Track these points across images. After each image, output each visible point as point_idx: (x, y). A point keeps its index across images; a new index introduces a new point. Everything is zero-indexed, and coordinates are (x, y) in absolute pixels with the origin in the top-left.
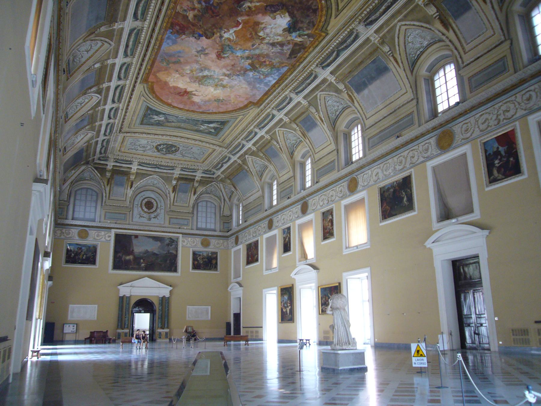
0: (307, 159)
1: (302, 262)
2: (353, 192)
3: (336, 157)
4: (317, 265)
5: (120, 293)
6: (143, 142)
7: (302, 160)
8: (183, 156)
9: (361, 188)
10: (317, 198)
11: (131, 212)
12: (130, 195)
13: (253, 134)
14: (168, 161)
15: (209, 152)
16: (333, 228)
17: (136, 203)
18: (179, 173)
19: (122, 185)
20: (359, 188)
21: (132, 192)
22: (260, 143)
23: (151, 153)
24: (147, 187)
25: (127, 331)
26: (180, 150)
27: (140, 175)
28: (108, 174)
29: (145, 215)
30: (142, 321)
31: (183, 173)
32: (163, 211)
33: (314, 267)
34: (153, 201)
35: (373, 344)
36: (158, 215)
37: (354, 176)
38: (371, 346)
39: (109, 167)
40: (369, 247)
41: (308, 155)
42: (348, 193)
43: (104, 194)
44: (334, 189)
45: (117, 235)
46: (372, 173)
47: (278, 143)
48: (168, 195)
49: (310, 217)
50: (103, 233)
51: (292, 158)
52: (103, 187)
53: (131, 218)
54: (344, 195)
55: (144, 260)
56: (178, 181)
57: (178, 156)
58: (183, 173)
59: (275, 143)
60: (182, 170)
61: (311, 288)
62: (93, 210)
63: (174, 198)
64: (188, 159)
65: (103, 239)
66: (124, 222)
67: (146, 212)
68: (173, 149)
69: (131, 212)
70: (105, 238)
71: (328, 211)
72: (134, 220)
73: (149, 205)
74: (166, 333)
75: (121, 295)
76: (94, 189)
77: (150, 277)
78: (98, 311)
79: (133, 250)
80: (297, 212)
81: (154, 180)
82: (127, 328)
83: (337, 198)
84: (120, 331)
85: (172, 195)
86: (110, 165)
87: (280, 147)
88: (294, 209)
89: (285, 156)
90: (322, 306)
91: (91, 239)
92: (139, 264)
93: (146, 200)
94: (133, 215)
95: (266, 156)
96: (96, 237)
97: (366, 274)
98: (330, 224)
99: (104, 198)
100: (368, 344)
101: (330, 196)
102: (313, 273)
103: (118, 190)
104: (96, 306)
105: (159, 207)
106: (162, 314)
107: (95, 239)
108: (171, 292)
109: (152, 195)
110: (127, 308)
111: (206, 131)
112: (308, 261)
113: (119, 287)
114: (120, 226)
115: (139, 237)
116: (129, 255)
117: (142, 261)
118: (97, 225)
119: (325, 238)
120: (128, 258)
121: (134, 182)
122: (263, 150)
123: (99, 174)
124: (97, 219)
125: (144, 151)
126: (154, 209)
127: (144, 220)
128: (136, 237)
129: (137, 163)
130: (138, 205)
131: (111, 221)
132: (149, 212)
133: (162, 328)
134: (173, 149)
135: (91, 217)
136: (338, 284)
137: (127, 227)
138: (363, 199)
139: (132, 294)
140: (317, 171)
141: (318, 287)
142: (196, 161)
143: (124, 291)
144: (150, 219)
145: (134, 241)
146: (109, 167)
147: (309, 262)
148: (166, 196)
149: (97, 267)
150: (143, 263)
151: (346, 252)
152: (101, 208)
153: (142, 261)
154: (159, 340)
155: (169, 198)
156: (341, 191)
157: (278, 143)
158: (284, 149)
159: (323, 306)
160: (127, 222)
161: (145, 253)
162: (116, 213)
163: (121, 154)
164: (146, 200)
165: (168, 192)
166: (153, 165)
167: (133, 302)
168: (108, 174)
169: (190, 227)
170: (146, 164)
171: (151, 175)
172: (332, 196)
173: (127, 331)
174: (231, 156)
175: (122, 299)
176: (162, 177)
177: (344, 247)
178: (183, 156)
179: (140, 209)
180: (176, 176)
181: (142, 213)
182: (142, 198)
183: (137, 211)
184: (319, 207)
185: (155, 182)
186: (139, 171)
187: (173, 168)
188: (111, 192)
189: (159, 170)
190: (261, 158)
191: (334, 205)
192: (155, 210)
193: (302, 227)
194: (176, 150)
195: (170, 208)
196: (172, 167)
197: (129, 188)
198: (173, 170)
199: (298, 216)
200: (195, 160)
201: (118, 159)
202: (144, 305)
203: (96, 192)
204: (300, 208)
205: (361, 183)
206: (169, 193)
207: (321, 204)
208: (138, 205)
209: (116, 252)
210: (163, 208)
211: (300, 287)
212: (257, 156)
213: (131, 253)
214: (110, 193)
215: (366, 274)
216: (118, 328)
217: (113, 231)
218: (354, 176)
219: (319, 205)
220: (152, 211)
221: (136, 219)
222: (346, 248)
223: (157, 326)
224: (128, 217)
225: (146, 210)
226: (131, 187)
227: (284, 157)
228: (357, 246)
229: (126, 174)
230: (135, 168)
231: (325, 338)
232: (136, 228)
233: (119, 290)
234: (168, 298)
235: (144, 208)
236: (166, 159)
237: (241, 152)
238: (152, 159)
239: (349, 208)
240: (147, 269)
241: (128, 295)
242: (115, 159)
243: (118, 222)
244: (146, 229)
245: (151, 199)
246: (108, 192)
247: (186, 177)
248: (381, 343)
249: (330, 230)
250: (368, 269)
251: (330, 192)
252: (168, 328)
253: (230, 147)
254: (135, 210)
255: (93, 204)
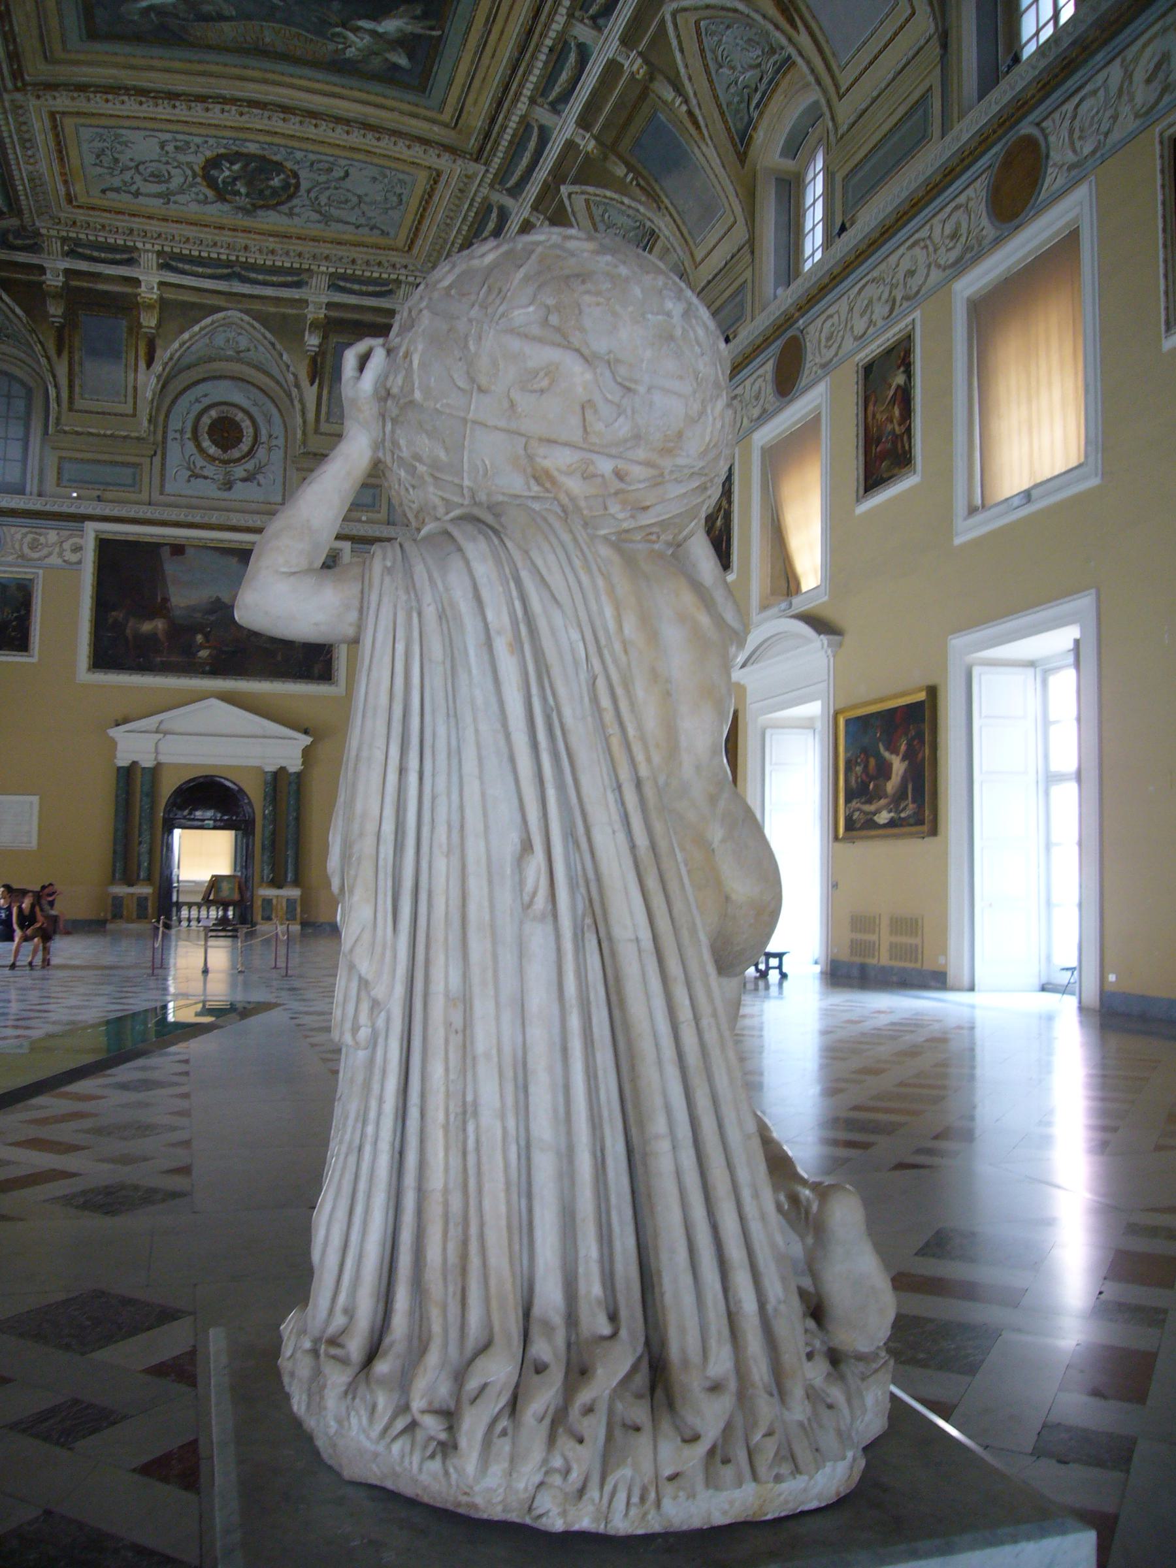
0: (812, 158)
1: (774, 611)
2: (1016, 215)
3: (935, 78)
4: (830, 614)
5: (119, 755)
6: (144, 147)
7: (789, 165)
8: (327, 219)
9: (1060, 181)
10: (843, 305)
11: (157, 460)
12: (149, 395)
13: (572, 57)
14: (271, 243)
15: (419, 192)
16: (909, 430)
17: (175, 424)
18: (324, 299)
19: (112, 352)
20: (1053, 179)
21: (153, 380)
22: (608, 108)
23: (194, 207)
24: (216, 365)
25: (145, 890)
26: (305, 185)
27: (179, 311)
28: (55, 310)
29: (210, 470)
30: (202, 856)
31: (340, 298)
32: (277, 455)
33: (819, 623)
34: (240, 416)
35: (1091, 994)
36: (259, 469)
37: (1026, 128)
38: (1081, 1009)
39: (53, 280)
40: (1094, 482)
41: (812, 139)
42: (990, 232)
43: (52, 392)
44: (924, 233)
45: (105, 546)
46: (1128, 76)
47: (679, 90)
48: (295, 392)
49: (813, 400)
50: (52, 536)
51: (742, 157)
52: (43, 361)
53: (156, 481)
54: (967, 249)
55: (206, 636)
56: (325, 337)
57: (300, 219)
58: (340, 298)
59: (668, 94)
60: (333, 287)
61: (807, 724)
62: (15, 450)
63: (319, 405)
64: (349, 234)
65: (54, 560)
66: (133, 497)
67: (212, 459)
68: (276, 182)
69: (157, 460)
70: (60, 555)
71: (889, 352)
72: (169, 488)
73: (225, 432)
74: (291, 902)
75: (123, 761)
76: (18, 372)
77: (229, 698)
78: (40, 819)
79: (166, 600)
80: (757, 398)
81: (230, 332)
82: (149, 880)
83: (936, 275)
84: (121, 890)
85: (310, 393)
86: (55, 267)
87: (690, 113)
88: (748, 383)
89: (711, 153)
90: (848, 800)
91: (10, 558)
92: (189, 650)
93: (213, 413)
94: (163, 465)
95: (638, 174)
96: (26, 550)
97: (1071, 633)
98: (897, 412)
99: (53, 405)
100: (1064, 990)
101: (900, 275)
102: (813, 654)
103: (99, 372)
104: (35, 799)
105: (264, 438)
106: (274, 833)
107: (23, 556)
108: (307, 752)
109: (238, 397)
110: (150, 808)
111: (376, 63)
112: (796, 601)
113: (114, 732)
114: (117, 511)
115: (190, 552)
116: (151, 617)
117: (199, 638)
118: (30, 506)
119: (872, 481)
120: (147, 627)
121: (159, 342)
122: (626, 144)
123: (18, 310)
124: (32, 485)
125: (166, 196)
126: (245, 447)
127: (208, 489)
128: (178, 549)
129: (152, 258)
130: (182, 432)
131: (84, 492)
132: (225, 457)
133: (277, 883)
134: (276, 182)
135: (8, 479)
136: (922, 696)
137: (141, 515)
138: (1072, 238)
139: (163, 759)
140: (846, 178)
141: (836, 714)
142: (382, 241)
143: (134, 746)
144: (228, 485)
145: (171, 567)
146: (53, 280)
147: (799, 604)
148: (289, 395)
149: (35, 660)
150: (202, 647)
151: (967, 531)
152: (43, 441)
153: (199, 638)
154: (263, 927)
155: (298, 406)
156: (954, 236)
157: (679, 90)
158: (707, 113)
159: (855, 804)
160: (144, 496)
161: (212, 611)
162: (99, 462)
163: (81, 216)
164: (213, 413)
165: (291, 378)
166: (218, 263)
167: (168, 787)
168: (55, 310)
169: (383, 515)
170: (191, 260)
171: (220, 309)
172: (911, 273)
173: (145, 890)
174: (508, 202)
175: (127, 774)
176: (263, 319)
177: (960, 506)
178: (327, 219)
179: (190, 447)
180: (315, 313)
181: (200, 462)
182: (198, 407)
183: (178, 453)
184: (849, 344)
185: (243, 342)
186: (170, 295)
187: (297, 278)
188: (77, 382)
189: (246, 289)
190: (623, 189)
191: (917, 314)
192: (250, 453)
193: (779, 459)
194: (286, 186)
195: (304, 443)
196: (291, 271)
197: (142, 365)
198: (298, 285)
199: (764, 411)
200: (374, 238)
201: (77, 242)
202: (208, 798)
203: (23, 383)
204: (769, 376)
205: (1060, 154)
206: (297, 386)
207: (860, 325)
208: (182, 432)
209: (102, 605)
210: (280, 442)
211: (763, 719)
212: (604, 180)
213: (161, 609)
214: (71, 386)
215: (1071, 633)
216: (113, 881)
217: (91, 528)
218: (1026, 128)
219: (846, 338)
220: (235, 453)
221: (178, 484)
222: (972, 510)
223: (257, 878)
224: (146, 480)
225: (213, 450)
226: (150, 363)
227: (709, 157)
228: (1027, 495)
229: (124, 305)
230: (150, 280)
231: (857, 947)
232: (174, 518)
233: (113, 744)
234: (299, 775)
235: (206, 443)
236: (263, 236)
237: (542, 174)
238: (207, 235)
239: (991, 314)
240: (217, 669)
241: (147, 762)
242: (64, 240)
243: (109, 495)
244: (214, 520)
245: (235, 411)
246: (63, 382)
247: (356, 316)
248: (1144, 998)
249: (896, 438)
250: (1085, 602)
251: (900, 258)
252: (297, 883)
253: (494, 149)
254: (174, 449)
255: (16, 430)
